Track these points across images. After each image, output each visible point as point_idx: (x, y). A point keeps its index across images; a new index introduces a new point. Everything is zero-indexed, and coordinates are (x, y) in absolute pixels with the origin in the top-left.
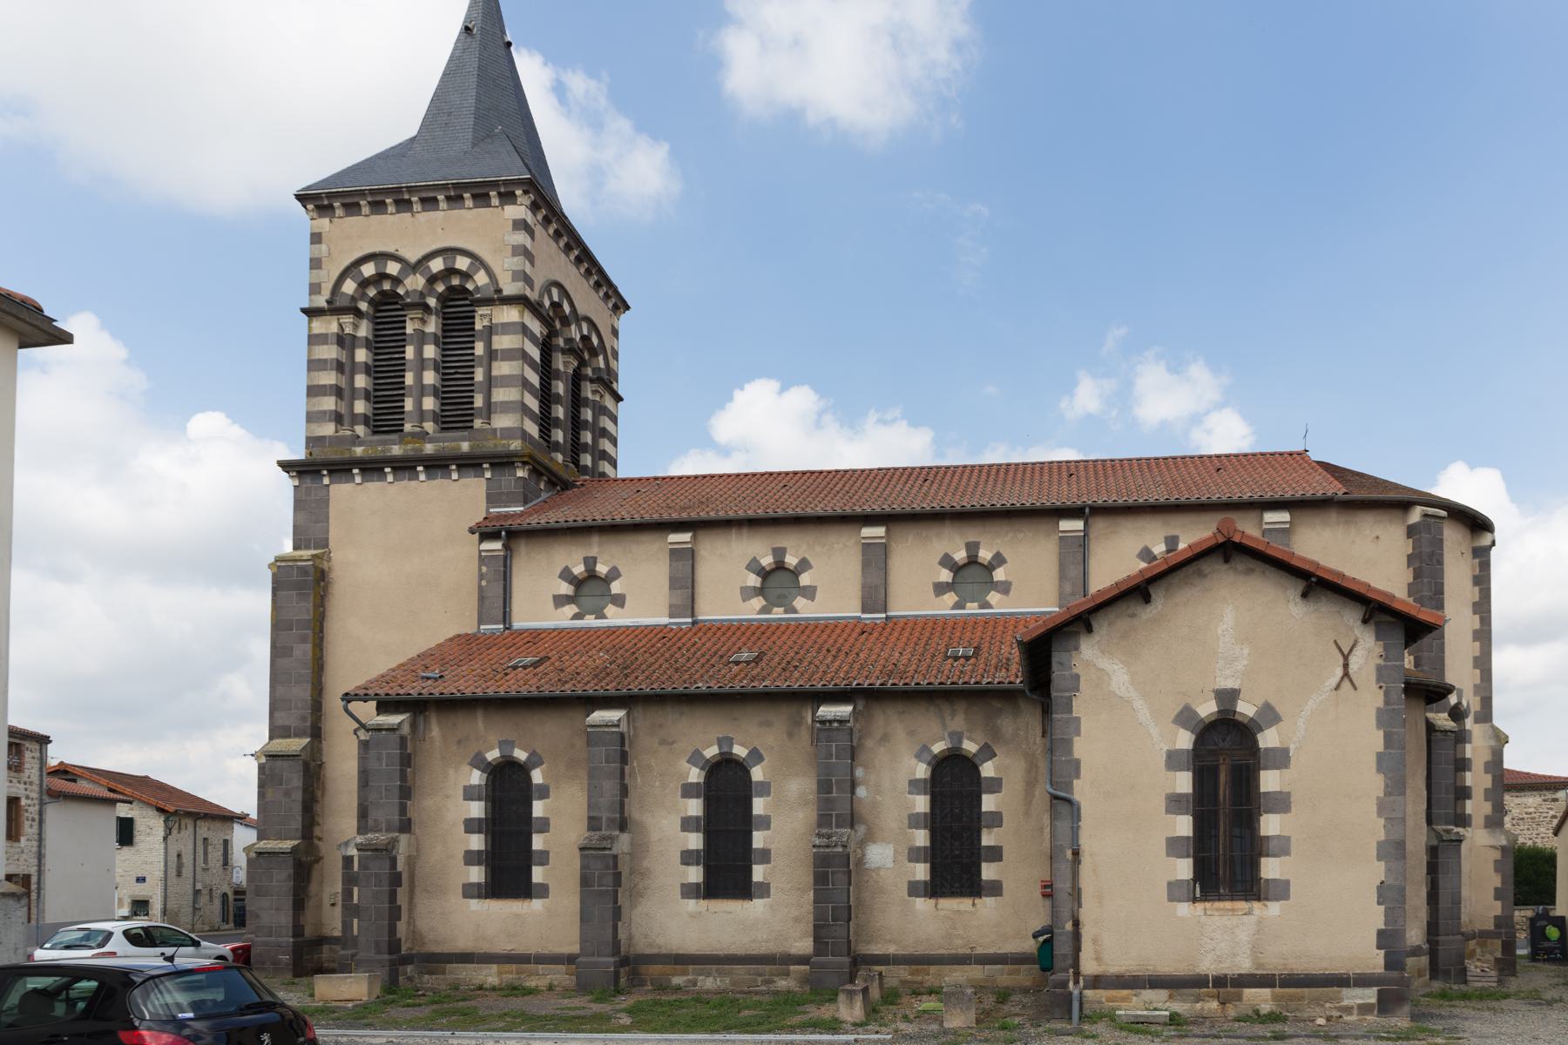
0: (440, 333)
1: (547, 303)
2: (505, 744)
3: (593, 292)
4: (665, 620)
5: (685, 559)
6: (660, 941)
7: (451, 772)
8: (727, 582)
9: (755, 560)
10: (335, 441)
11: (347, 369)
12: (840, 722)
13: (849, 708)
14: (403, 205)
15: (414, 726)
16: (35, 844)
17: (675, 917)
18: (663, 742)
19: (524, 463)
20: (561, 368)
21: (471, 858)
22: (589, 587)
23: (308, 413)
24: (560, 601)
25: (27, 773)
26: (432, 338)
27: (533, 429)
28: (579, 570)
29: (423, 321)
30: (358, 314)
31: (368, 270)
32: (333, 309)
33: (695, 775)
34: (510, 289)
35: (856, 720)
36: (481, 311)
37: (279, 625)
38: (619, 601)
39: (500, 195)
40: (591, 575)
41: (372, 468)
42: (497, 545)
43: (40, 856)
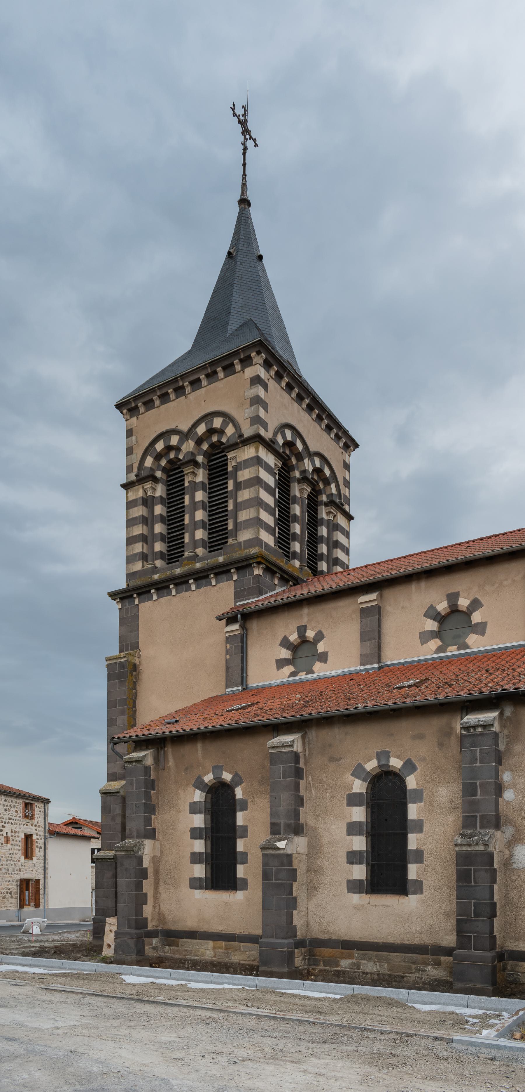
1: (280, 441)
2: (217, 769)
3: (325, 435)
4: (358, 668)
5: (374, 615)
6: (331, 928)
7: (182, 793)
8: (408, 634)
9: (432, 607)
10: (143, 573)
11: (149, 521)
12: (484, 726)
13: (495, 714)
14: (180, 391)
15: (157, 759)
16: (43, 861)
17: (338, 905)
18: (332, 759)
19: (259, 563)
20: (297, 494)
21: (195, 858)
22: (302, 650)
24: (281, 663)
25: (36, 820)
26: (200, 486)
28: (294, 637)
29: (195, 474)
30: (155, 480)
31: (160, 446)
32: (140, 480)
33: (359, 786)
34: (248, 432)
35: (503, 726)
36: (231, 455)
37: (111, 704)
38: (323, 657)
41: (162, 587)
42: (236, 627)
43: (45, 869)
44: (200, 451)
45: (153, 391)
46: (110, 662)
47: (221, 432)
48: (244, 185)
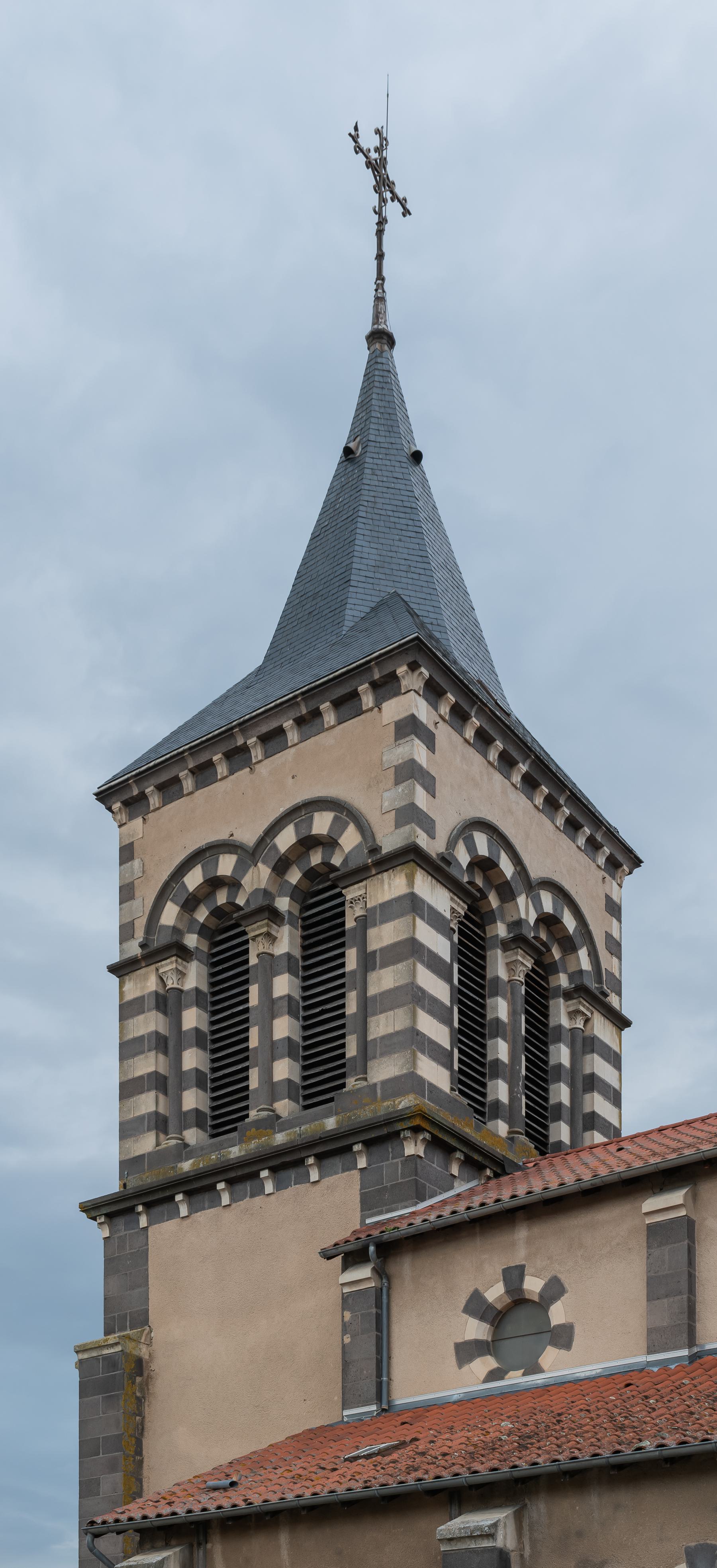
0: (297, 953)
1: (463, 857)
3: (564, 841)
4: (642, 1359)
11: (171, 1044)
14: (238, 757)
19: (416, 1130)
20: (503, 974)
23: (122, 1125)
24: (467, 1352)
27: (438, 1076)
28: (495, 1293)
29: (271, 938)
30: (184, 953)
31: (194, 879)
32: (152, 955)
34: (390, 840)
39: (375, 686)
40: (518, 1300)
41: (199, 1188)
42: (364, 1272)
44: (283, 888)
45: (178, 759)
46: (85, 1356)
47: (330, 843)
48: (380, 300)
